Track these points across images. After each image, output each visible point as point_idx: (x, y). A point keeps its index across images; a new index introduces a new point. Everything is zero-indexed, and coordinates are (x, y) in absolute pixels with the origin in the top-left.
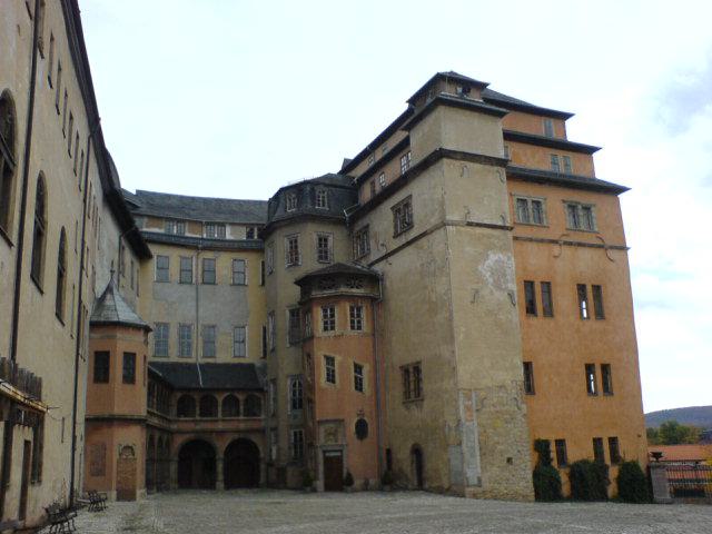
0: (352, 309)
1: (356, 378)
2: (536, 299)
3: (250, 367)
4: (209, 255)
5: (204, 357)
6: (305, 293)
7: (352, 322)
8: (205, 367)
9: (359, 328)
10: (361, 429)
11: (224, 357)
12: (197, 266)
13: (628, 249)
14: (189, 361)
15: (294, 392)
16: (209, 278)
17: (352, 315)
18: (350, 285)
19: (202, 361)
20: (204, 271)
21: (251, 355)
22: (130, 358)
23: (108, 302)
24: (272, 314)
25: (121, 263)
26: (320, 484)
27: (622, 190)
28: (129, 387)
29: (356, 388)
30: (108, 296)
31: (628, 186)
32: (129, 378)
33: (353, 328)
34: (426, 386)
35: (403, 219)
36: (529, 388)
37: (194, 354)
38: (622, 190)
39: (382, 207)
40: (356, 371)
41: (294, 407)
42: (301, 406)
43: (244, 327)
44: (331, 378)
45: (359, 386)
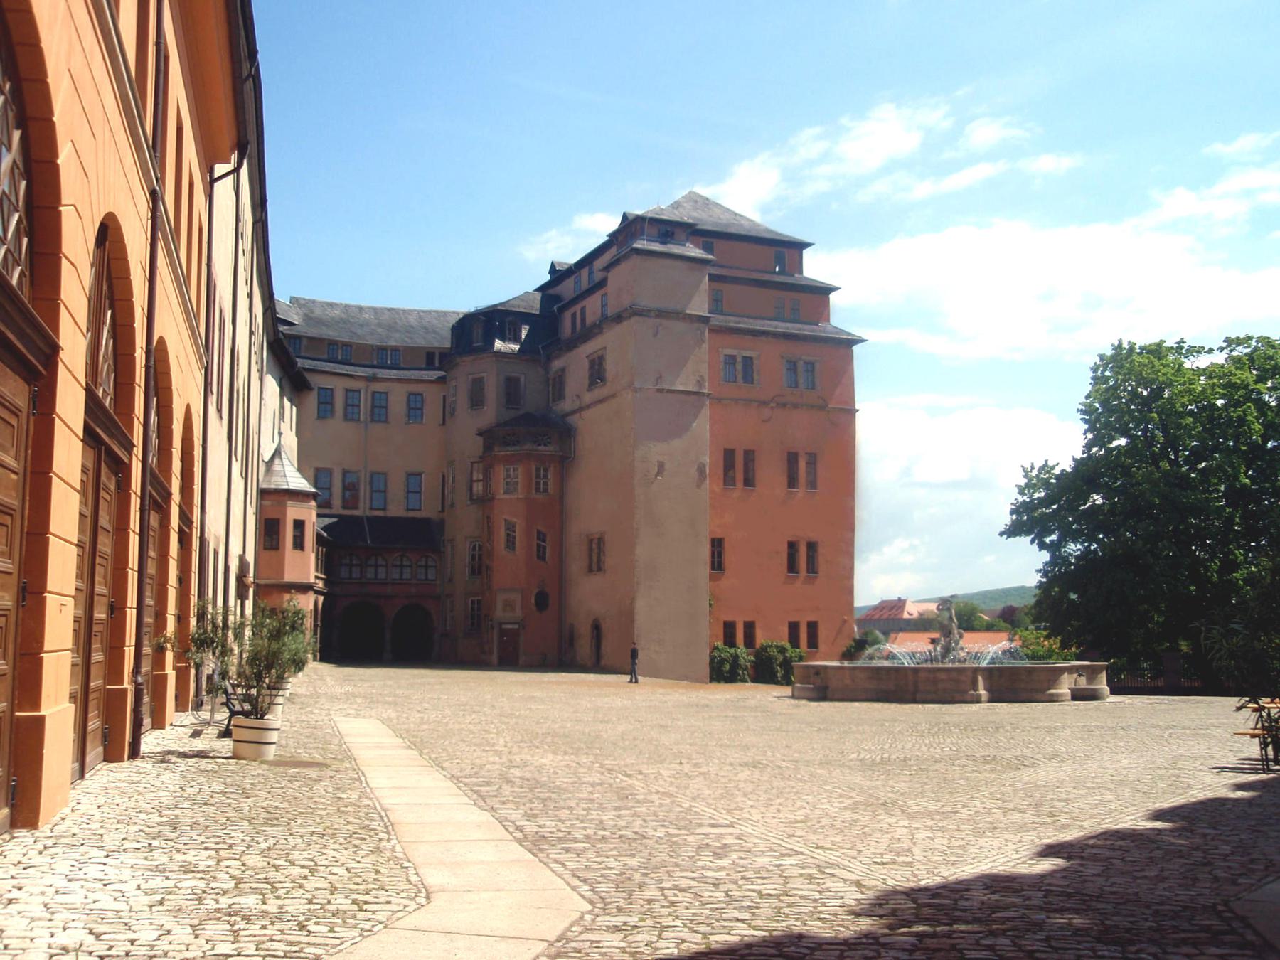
0: (538, 470)
1: (538, 545)
2: (737, 467)
3: (426, 521)
4: (378, 387)
5: (371, 509)
6: (488, 448)
7: (538, 483)
8: (371, 520)
9: (546, 490)
10: (542, 601)
11: (396, 509)
12: (366, 400)
13: (823, 291)
14: (356, 513)
15: (473, 556)
16: (379, 411)
17: (538, 476)
18: (535, 431)
19: (368, 513)
20: (373, 407)
21: (428, 509)
22: (299, 525)
23: (277, 466)
24: (451, 463)
25: (282, 407)
26: (495, 658)
28: (298, 552)
29: (538, 557)
30: (277, 461)
32: (299, 544)
33: (537, 490)
34: (609, 561)
35: (597, 373)
36: (717, 563)
37: (361, 505)
39: (575, 352)
40: (538, 539)
41: (473, 572)
42: (480, 573)
43: (420, 474)
45: (541, 556)
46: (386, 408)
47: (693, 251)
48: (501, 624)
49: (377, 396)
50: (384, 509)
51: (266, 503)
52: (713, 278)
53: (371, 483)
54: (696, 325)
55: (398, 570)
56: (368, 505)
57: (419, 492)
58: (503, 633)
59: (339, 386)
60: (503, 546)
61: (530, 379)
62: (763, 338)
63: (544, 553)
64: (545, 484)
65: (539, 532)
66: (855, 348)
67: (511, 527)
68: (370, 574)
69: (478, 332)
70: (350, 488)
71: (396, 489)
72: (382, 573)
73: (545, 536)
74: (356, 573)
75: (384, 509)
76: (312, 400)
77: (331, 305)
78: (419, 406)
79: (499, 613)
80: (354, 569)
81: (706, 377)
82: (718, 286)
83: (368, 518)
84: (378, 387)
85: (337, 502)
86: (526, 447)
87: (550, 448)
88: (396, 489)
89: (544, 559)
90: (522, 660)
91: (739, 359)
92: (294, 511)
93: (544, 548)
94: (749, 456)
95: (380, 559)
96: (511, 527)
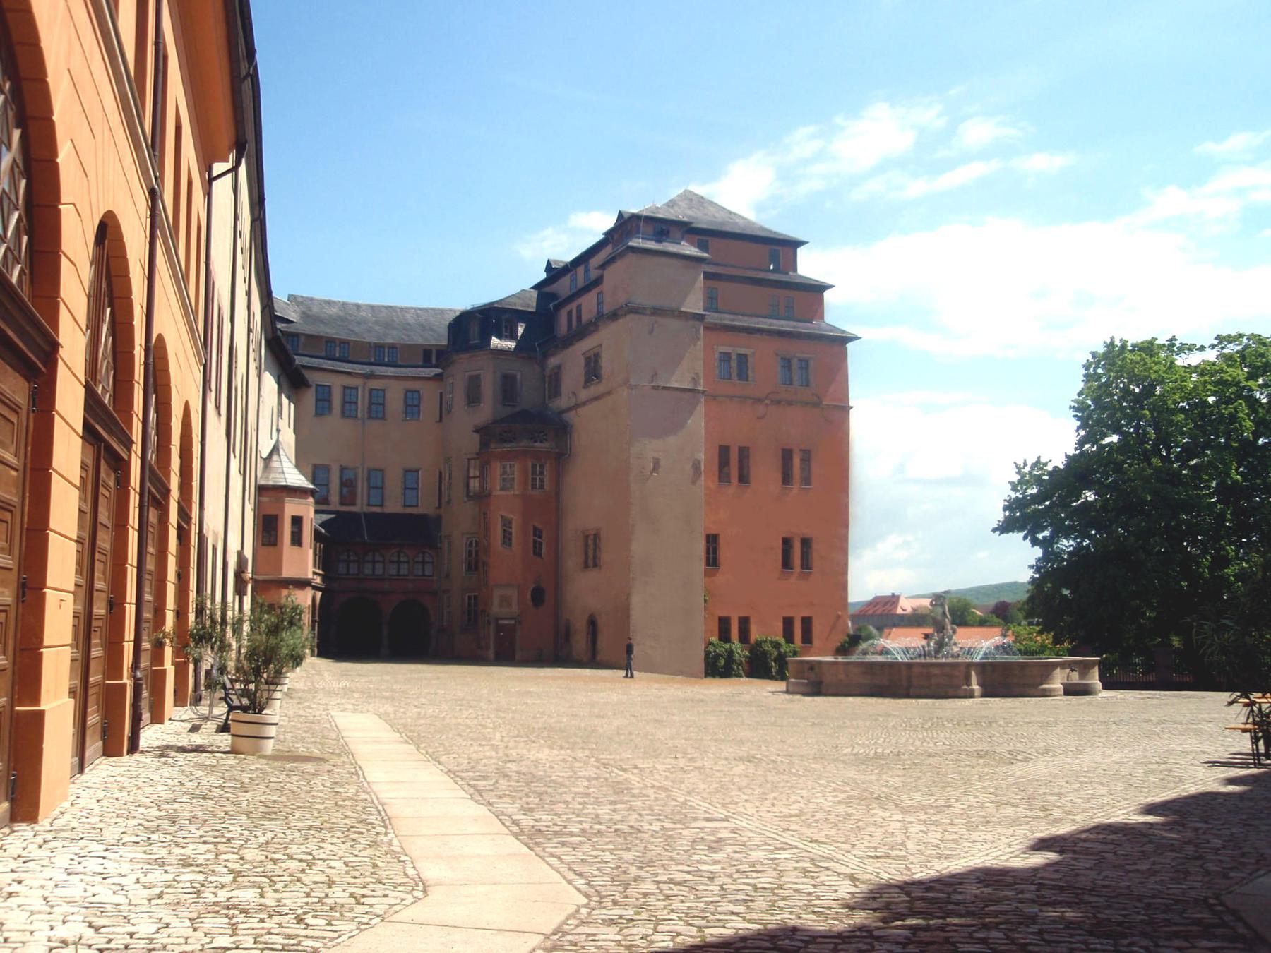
0: (534, 466)
1: (535, 541)
2: (732, 464)
3: (423, 517)
4: (375, 384)
5: (369, 505)
6: (484, 444)
7: (534, 480)
8: (369, 516)
9: (542, 487)
10: (538, 596)
11: (393, 506)
12: (363, 397)
14: (353, 509)
15: (470, 552)
16: (377, 408)
17: (534, 473)
18: (531, 428)
19: (366, 509)
20: (371, 404)
21: (425, 505)
22: (297, 521)
23: (275, 463)
24: (448, 460)
25: (280, 404)
26: (491, 653)
27: (799, 243)
28: (296, 548)
29: (535, 553)
30: (275, 458)
31: (801, 237)
32: (297, 540)
33: (534, 486)
34: (605, 557)
35: (593, 370)
36: (712, 559)
37: (359, 501)
38: (799, 243)
39: (571, 349)
40: (535, 535)
41: (469, 568)
42: (476, 569)
43: (417, 471)
44: (507, 538)
45: (537, 552)
46: (383, 405)
47: (688, 249)
48: (497, 619)
49: (375, 393)
50: (382, 506)
51: (264, 499)
52: (708, 276)
53: (369, 479)
54: (691, 323)
55: (396, 566)
56: (365, 502)
57: (416, 489)
58: (499, 628)
59: (336, 383)
60: (499, 542)
61: (527, 376)
62: (758, 336)
63: (540, 549)
64: (542, 480)
65: (535, 528)
66: (849, 346)
67: (507, 523)
68: (368, 569)
69: (474, 330)
70: (348, 485)
71: (394, 485)
72: (379, 569)
73: (541, 532)
74: (353, 569)
75: (382, 506)
76: (310, 397)
77: (329, 303)
78: (416, 403)
79: (495, 609)
80: (351, 565)
81: (701, 375)
82: (712, 283)
83: (365, 514)
84: (375, 384)
85: (334, 498)
86: (522, 444)
87: (546, 445)
88: (394, 485)
89: (540, 555)
90: (518, 655)
91: (734, 357)
92: (292, 508)
93: (540, 544)
94: (744, 453)
95: (377, 555)
96: (507, 523)
